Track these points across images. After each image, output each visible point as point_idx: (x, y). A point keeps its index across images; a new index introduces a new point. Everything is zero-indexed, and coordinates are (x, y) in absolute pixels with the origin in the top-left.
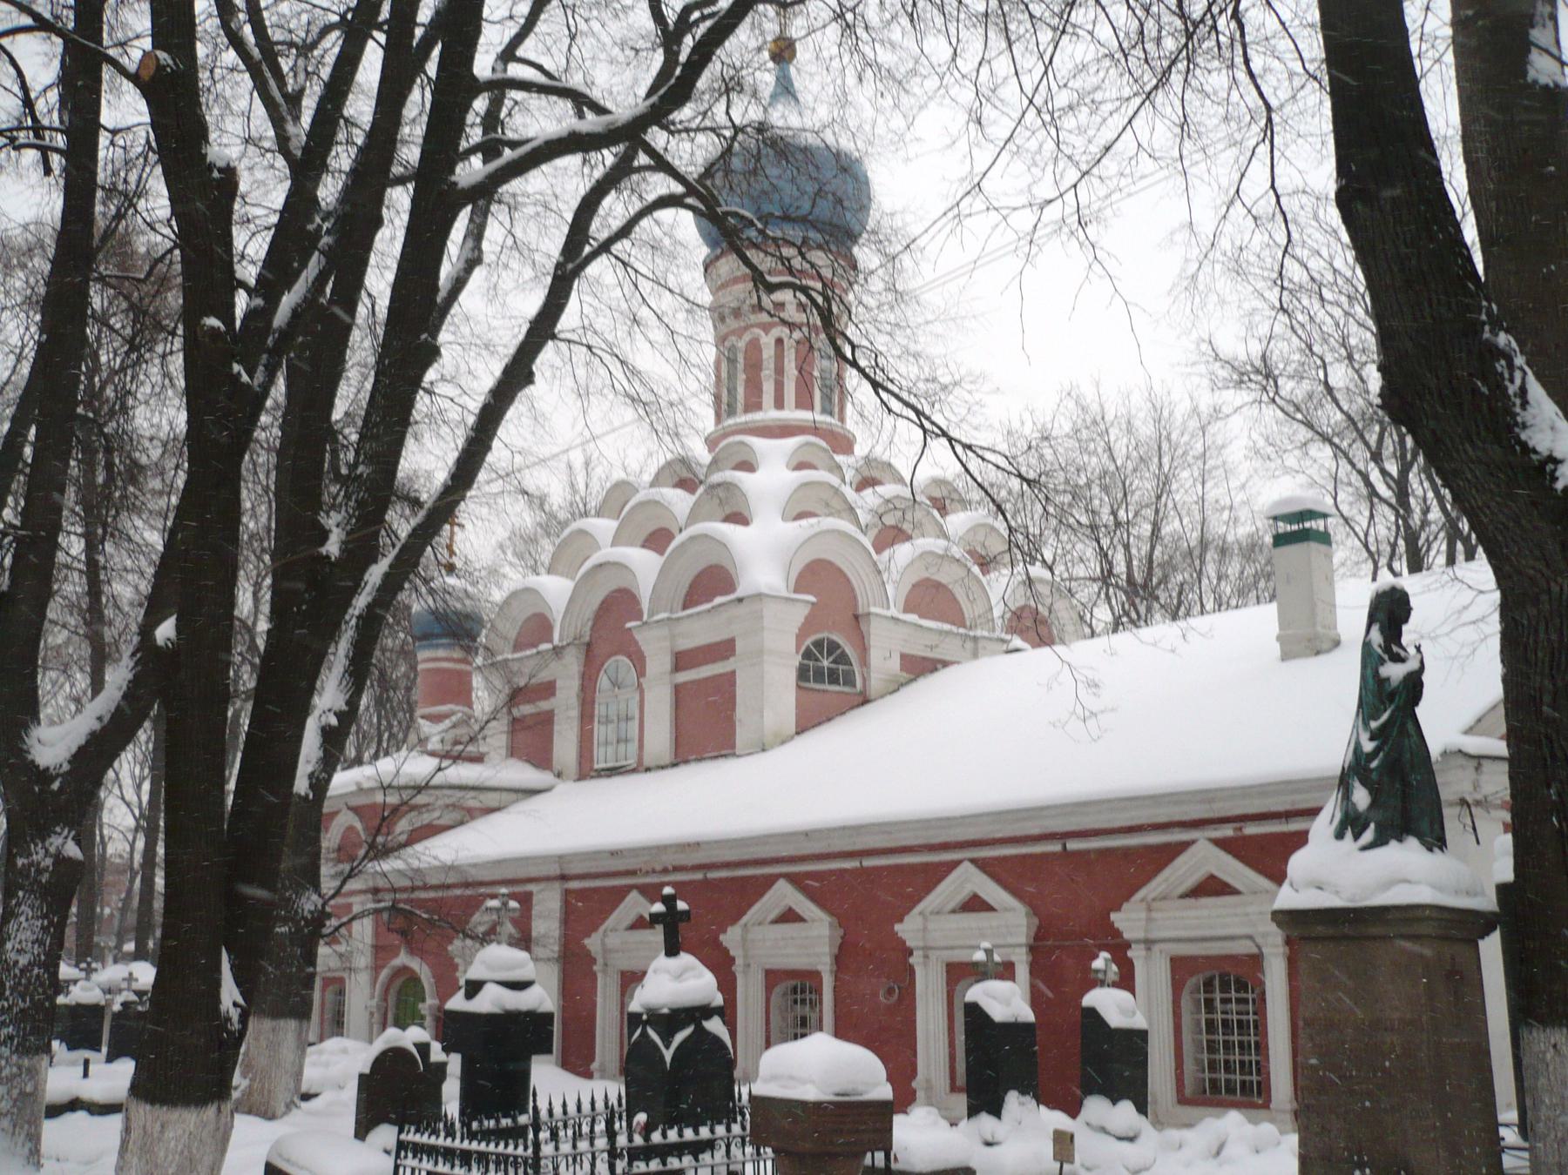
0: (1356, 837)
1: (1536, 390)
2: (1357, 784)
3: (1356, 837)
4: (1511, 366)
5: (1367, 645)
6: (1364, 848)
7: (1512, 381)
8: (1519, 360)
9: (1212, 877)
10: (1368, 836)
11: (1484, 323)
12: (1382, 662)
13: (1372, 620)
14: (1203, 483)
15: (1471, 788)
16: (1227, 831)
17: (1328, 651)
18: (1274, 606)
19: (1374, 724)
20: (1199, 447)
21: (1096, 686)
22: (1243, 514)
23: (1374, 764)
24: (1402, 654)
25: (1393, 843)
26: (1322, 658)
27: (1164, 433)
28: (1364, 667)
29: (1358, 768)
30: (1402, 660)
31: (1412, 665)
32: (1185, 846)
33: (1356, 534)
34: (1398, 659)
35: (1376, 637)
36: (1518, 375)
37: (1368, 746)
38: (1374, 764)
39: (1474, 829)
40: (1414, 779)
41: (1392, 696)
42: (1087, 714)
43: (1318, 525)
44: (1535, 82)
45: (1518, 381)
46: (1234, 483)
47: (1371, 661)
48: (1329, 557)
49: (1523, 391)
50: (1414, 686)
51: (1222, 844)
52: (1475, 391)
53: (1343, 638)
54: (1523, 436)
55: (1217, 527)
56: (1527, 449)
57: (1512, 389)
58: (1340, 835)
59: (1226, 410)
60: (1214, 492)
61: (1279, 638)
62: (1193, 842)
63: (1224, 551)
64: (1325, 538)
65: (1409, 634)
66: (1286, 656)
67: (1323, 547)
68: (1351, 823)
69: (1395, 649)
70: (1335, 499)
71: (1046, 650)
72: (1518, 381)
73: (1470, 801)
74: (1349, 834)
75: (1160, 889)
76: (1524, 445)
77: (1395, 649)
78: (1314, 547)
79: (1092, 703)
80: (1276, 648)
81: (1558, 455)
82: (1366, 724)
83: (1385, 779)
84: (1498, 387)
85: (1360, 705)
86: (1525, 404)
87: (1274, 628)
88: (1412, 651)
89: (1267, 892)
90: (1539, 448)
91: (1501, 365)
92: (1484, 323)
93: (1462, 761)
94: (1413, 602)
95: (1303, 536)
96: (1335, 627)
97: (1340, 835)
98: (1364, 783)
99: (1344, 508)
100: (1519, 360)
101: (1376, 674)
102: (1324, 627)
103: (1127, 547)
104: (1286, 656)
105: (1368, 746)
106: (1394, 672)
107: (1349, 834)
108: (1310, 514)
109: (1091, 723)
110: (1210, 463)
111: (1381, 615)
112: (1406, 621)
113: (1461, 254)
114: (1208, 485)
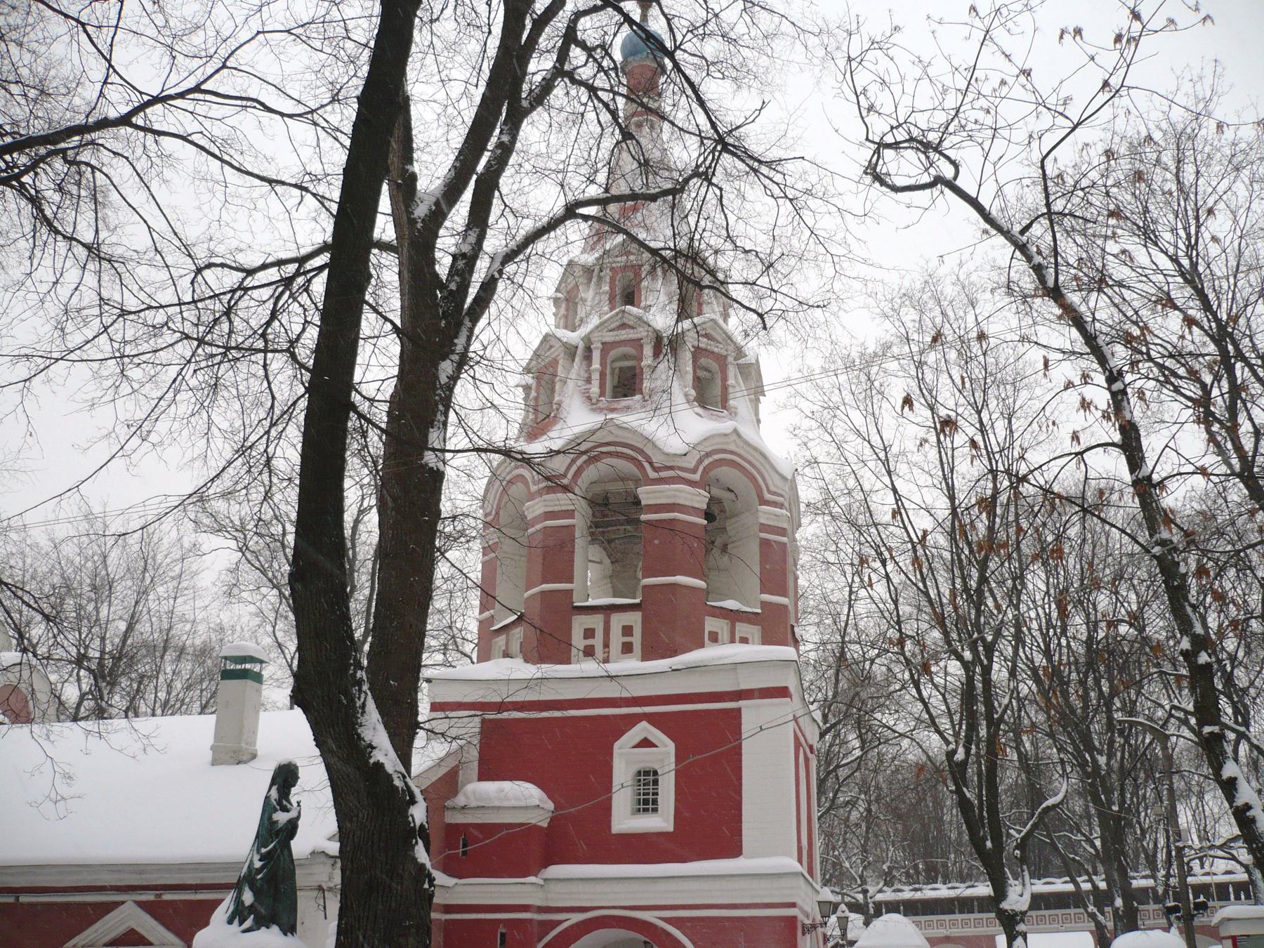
0: (241, 923)
1: (371, 705)
2: (247, 889)
3: (241, 923)
4: (360, 691)
5: (267, 798)
6: (244, 931)
7: (359, 699)
8: (365, 687)
9: (132, 932)
10: (249, 923)
11: (351, 665)
12: (276, 811)
13: (273, 783)
14: (175, 598)
15: (326, 879)
16: (149, 896)
17: (245, 762)
18: (209, 721)
19: (263, 850)
20: (177, 569)
21: (70, 777)
22: (201, 628)
23: (259, 877)
24: (289, 806)
25: (263, 929)
26: (241, 766)
27: (152, 554)
28: (264, 811)
29: (249, 879)
30: (288, 811)
31: (293, 814)
32: (117, 904)
33: (285, 657)
34: (285, 810)
35: (274, 794)
36: (363, 696)
37: (258, 864)
38: (259, 877)
39: (325, 908)
40: (282, 888)
41: (278, 833)
42: (59, 798)
43: (257, 668)
44: (427, 464)
45: (362, 700)
46: (199, 604)
47: (268, 810)
48: (259, 692)
49: (364, 705)
50: (292, 827)
51: (144, 906)
52: (340, 701)
53: (259, 753)
54: (359, 731)
55: (180, 629)
56: (360, 738)
57: (359, 704)
58: (230, 922)
59: (205, 548)
60: (182, 607)
61: (212, 748)
62: (123, 903)
63: (182, 651)
64: (258, 678)
65: (295, 794)
66: (215, 762)
67: (256, 684)
68: (239, 914)
69: (285, 802)
70: (274, 627)
71: (26, 729)
72: (362, 700)
73: (325, 888)
74: (236, 921)
75: (90, 938)
76: (359, 735)
77: (285, 802)
78: (250, 682)
79: (63, 789)
80: (209, 755)
81: (374, 744)
82: (258, 851)
83: (265, 886)
84: (352, 700)
85: (257, 837)
86: (363, 712)
87: (209, 740)
88: (295, 805)
89: (173, 944)
90: (366, 739)
91: (355, 690)
92: (351, 665)
93: (323, 859)
94: (301, 773)
95: (244, 675)
96: (255, 745)
97: (230, 922)
98: (251, 889)
99: (280, 635)
100: (365, 687)
101: (270, 818)
102: (247, 744)
103: (103, 639)
104: (215, 762)
105: (258, 864)
106: (281, 817)
107: (236, 921)
108: (252, 659)
109: (61, 804)
110: (184, 584)
111: (279, 780)
112: (294, 786)
113: (347, 625)
114: (178, 601)
